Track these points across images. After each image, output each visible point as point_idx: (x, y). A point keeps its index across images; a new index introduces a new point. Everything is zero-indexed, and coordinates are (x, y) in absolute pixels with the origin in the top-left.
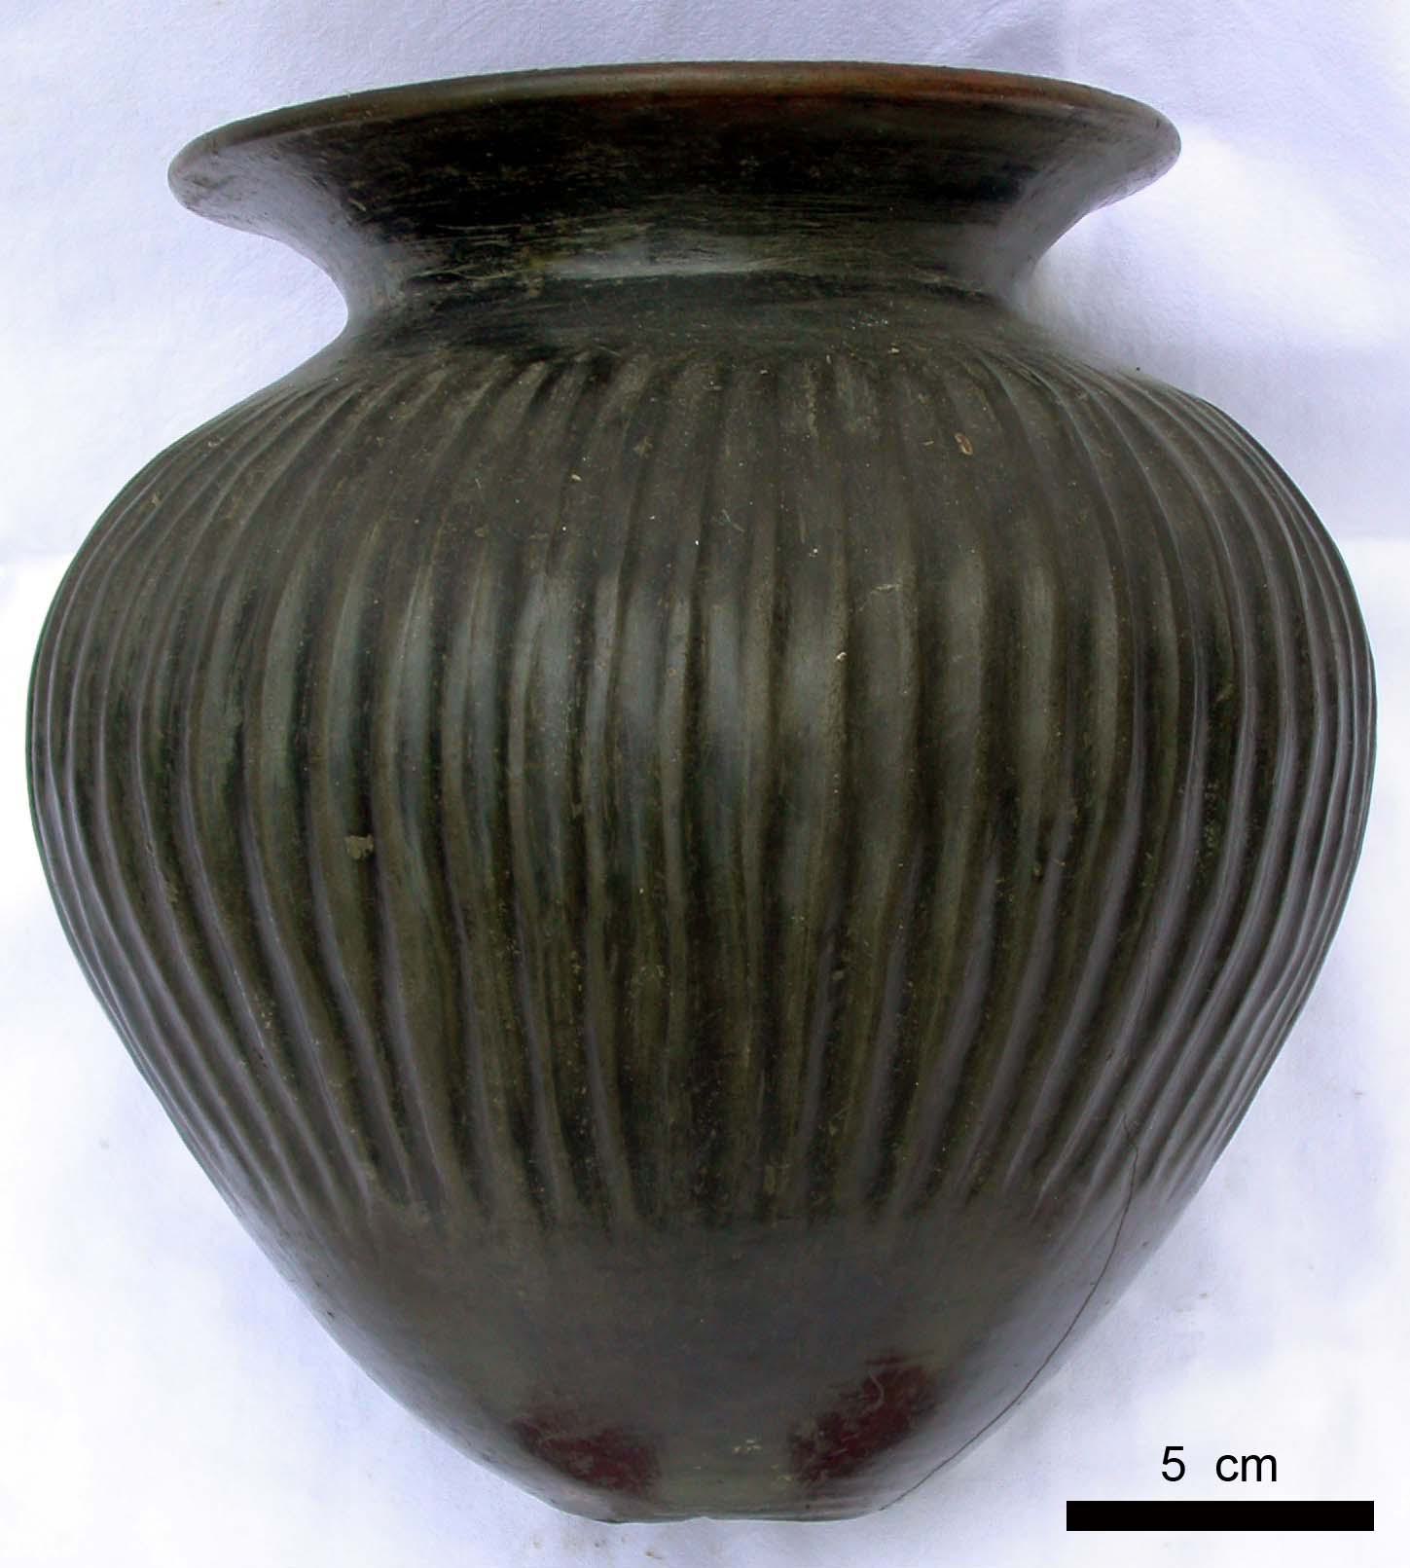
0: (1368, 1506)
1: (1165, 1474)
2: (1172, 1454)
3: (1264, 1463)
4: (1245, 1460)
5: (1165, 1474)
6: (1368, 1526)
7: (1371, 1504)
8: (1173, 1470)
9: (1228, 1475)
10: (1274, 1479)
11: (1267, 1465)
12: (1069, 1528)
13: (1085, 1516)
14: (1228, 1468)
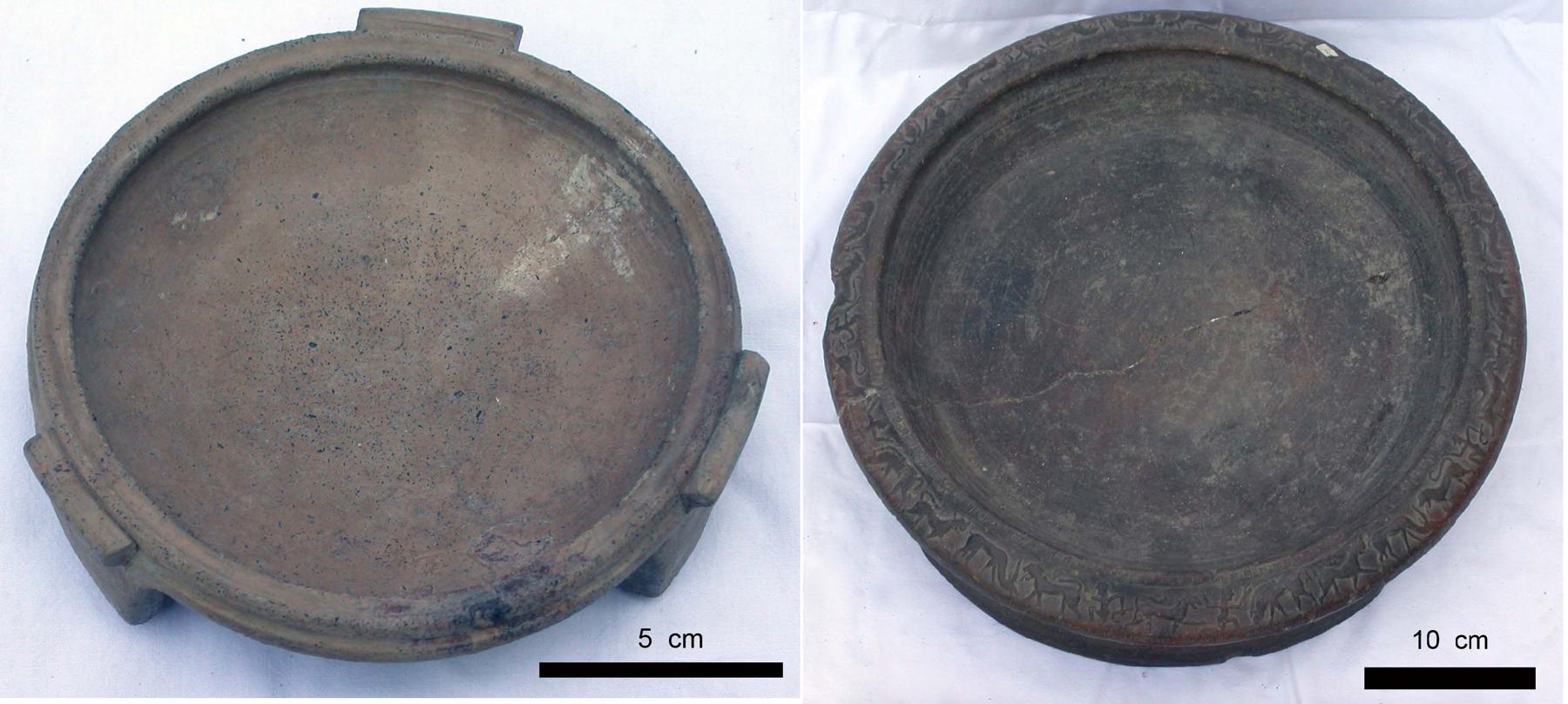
0: (1368, 686)
1: (640, 644)
2: (645, 633)
3: (695, 638)
4: (685, 636)
5: (640, 644)
6: (1531, 685)
7: (781, 664)
8: (645, 641)
9: (675, 644)
10: (701, 646)
11: (697, 639)
12: (1533, 687)
13: (1378, 678)
14: (675, 641)
